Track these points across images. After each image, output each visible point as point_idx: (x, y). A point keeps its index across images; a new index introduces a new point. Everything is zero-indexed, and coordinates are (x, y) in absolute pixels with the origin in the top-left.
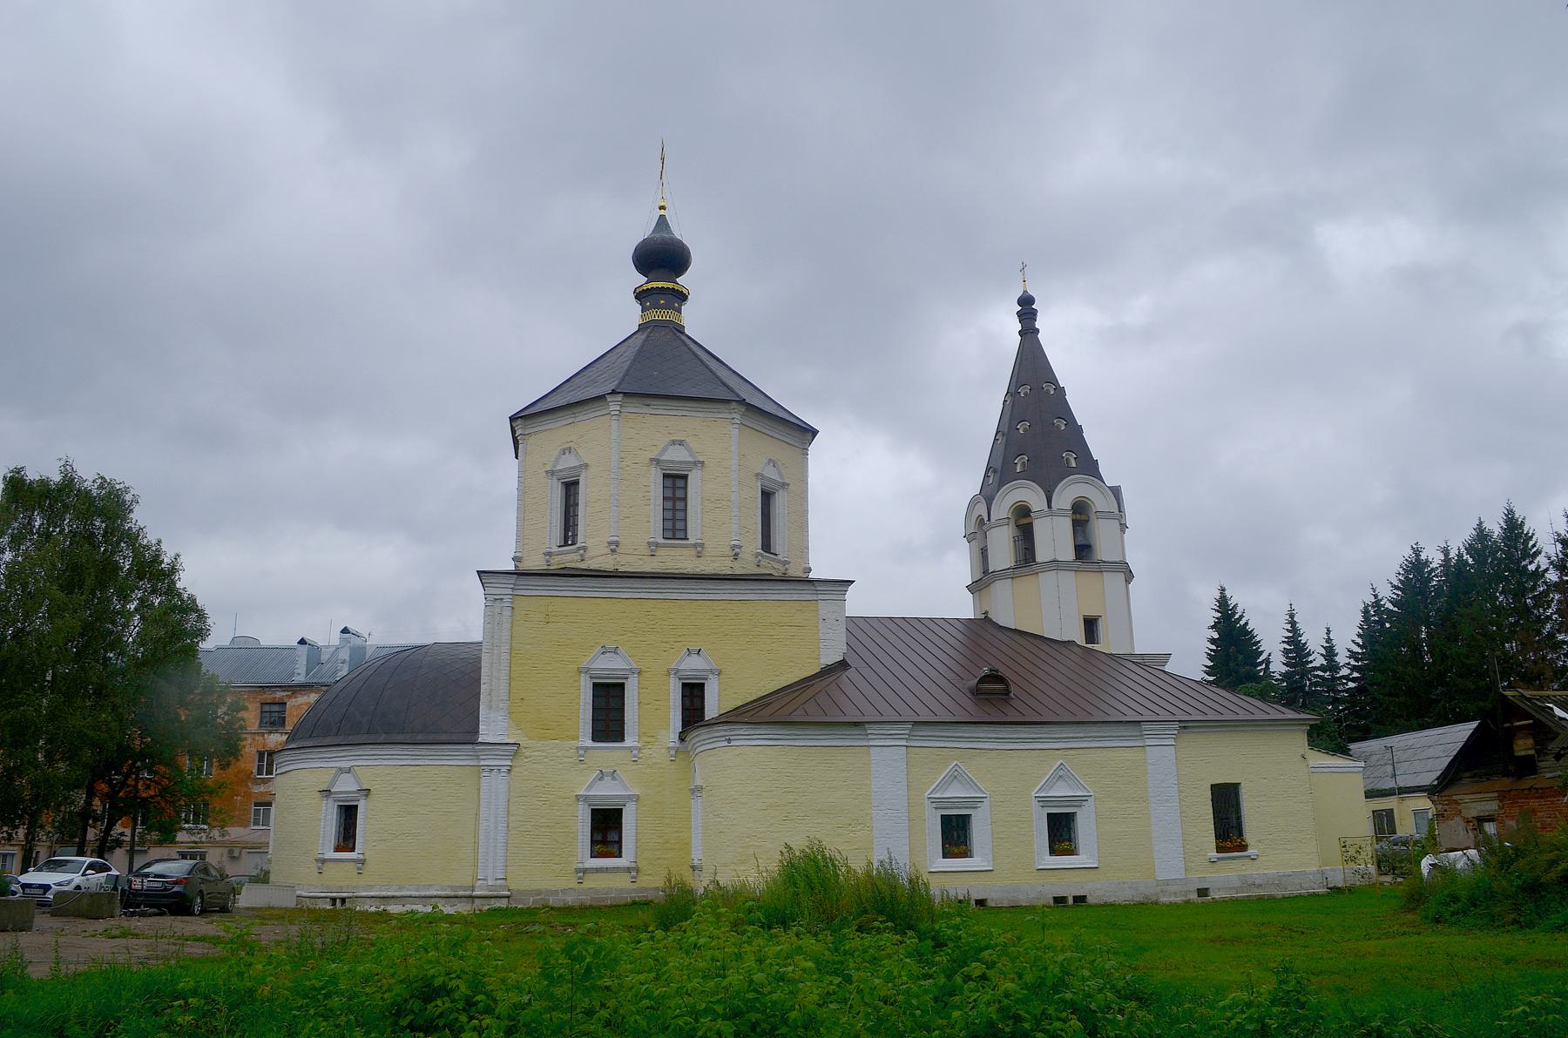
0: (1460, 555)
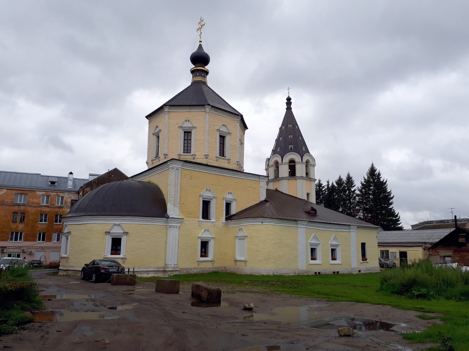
0: (333, 184)
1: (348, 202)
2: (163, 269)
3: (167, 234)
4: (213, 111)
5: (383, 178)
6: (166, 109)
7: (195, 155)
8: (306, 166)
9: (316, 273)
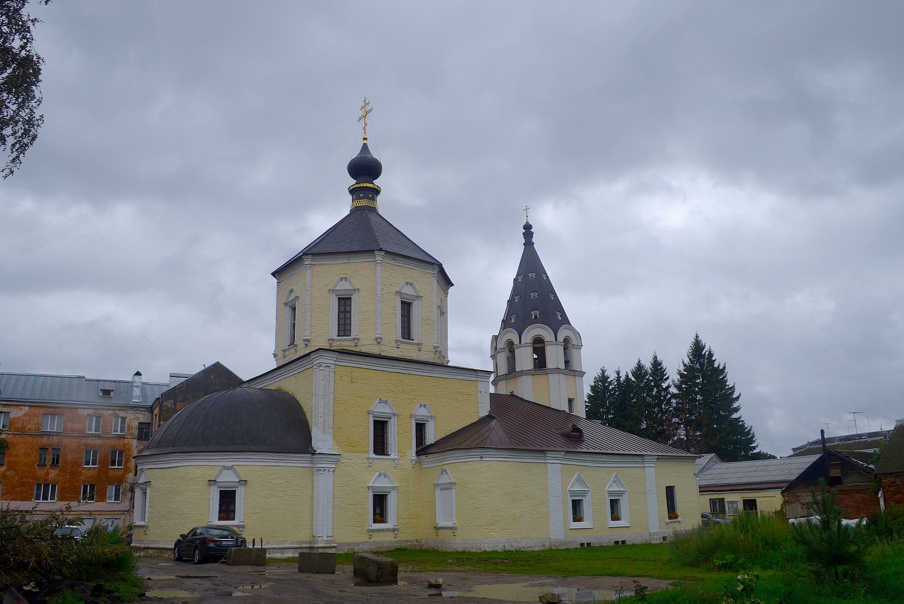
0: (627, 376)
1: (656, 410)
2: (308, 545)
3: (312, 482)
4: (388, 260)
5: (719, 360)
6: (307, 261)
7: (358, 339)
8: (565, 349)
9: (582, 545)
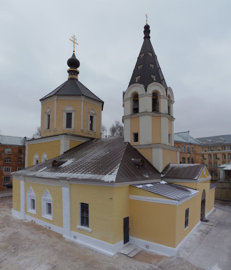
4: (87, 100)
